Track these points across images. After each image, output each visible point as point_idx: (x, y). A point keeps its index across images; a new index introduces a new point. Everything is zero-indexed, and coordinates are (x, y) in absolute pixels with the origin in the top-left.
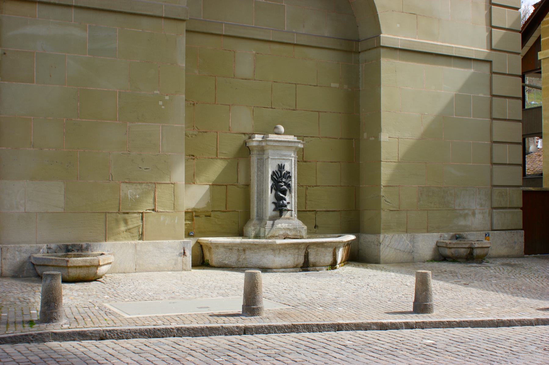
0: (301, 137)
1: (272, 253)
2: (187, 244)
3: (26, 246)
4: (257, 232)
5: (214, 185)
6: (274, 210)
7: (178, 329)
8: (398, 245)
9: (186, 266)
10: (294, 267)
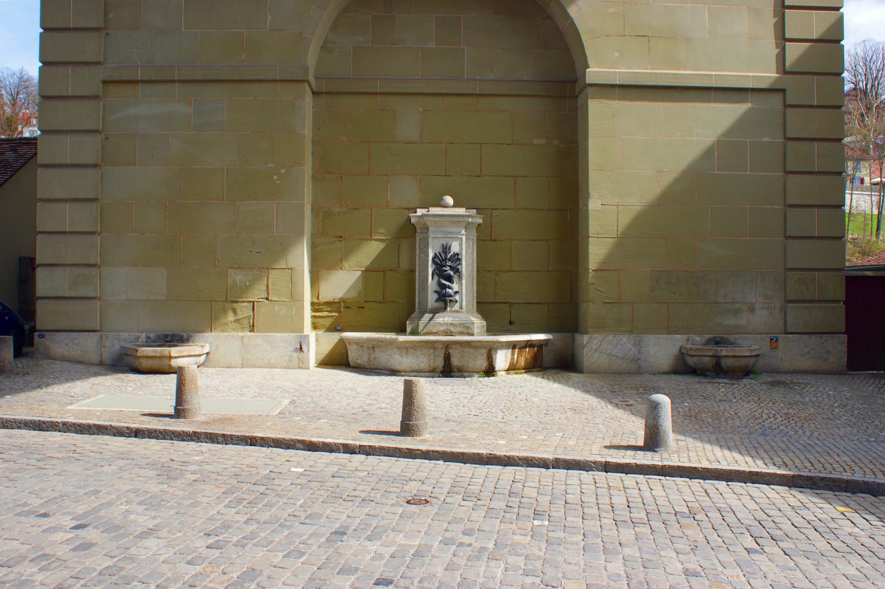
1: (398, 352)
3: (125, 335)
5: (368, 272)
6: (436, 301)
7: (64, 424)
8: (614, 348)
10: (430, 371)
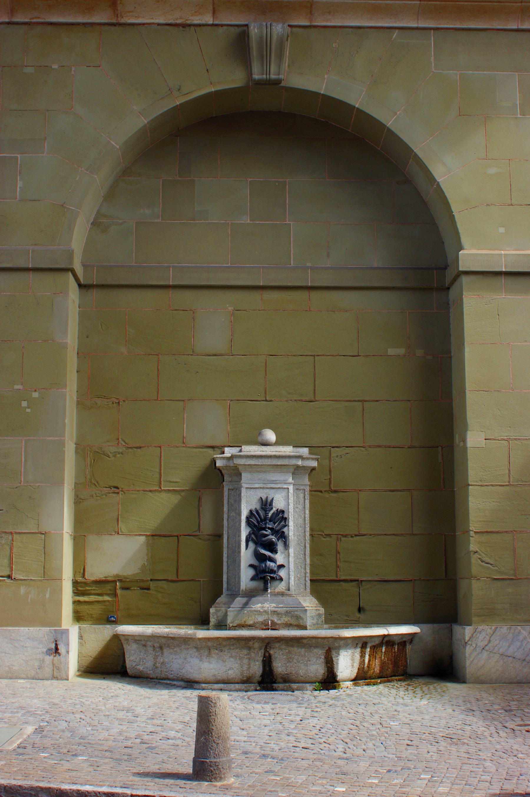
0: (323, 450)
1: (196, 654)
2: (62, 635)
4: (220, 618)
6: (253, 579)
8: (509, 646)
9: (60, 672)
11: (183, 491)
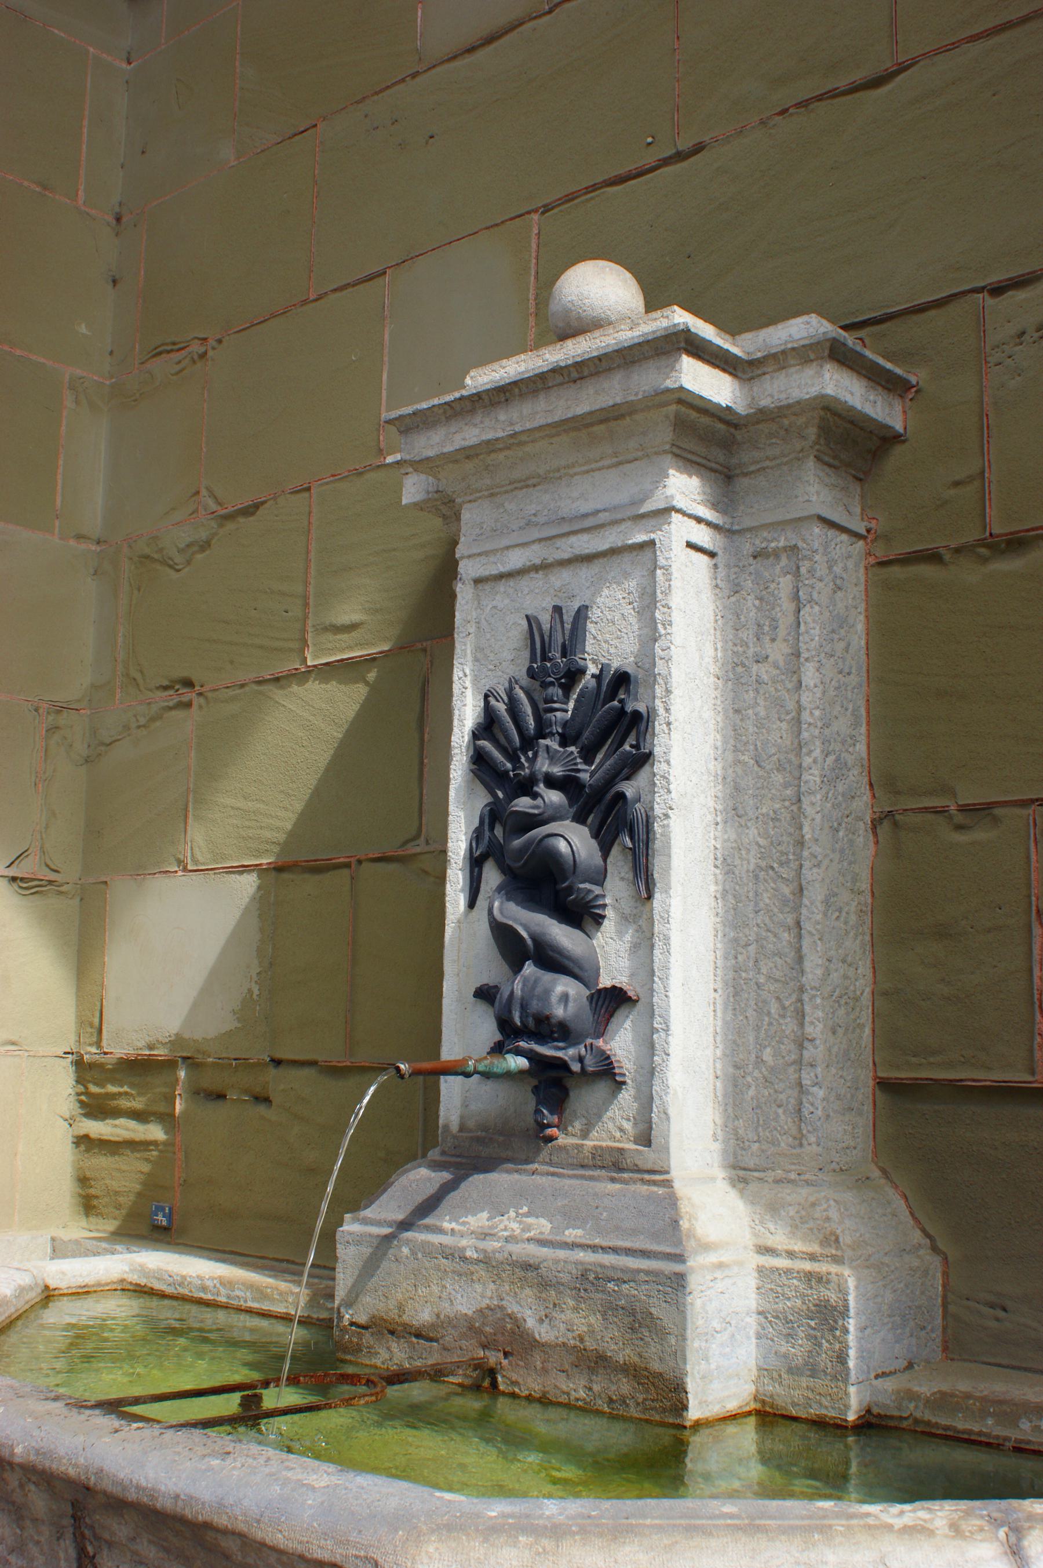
11: (372, 660)
